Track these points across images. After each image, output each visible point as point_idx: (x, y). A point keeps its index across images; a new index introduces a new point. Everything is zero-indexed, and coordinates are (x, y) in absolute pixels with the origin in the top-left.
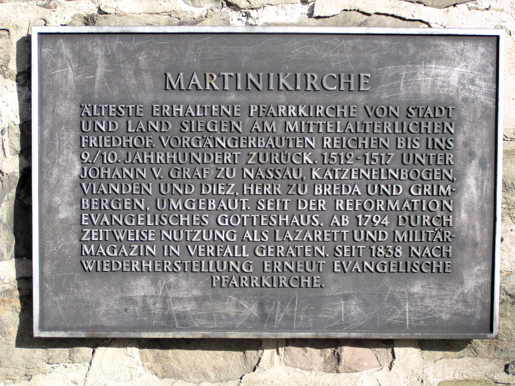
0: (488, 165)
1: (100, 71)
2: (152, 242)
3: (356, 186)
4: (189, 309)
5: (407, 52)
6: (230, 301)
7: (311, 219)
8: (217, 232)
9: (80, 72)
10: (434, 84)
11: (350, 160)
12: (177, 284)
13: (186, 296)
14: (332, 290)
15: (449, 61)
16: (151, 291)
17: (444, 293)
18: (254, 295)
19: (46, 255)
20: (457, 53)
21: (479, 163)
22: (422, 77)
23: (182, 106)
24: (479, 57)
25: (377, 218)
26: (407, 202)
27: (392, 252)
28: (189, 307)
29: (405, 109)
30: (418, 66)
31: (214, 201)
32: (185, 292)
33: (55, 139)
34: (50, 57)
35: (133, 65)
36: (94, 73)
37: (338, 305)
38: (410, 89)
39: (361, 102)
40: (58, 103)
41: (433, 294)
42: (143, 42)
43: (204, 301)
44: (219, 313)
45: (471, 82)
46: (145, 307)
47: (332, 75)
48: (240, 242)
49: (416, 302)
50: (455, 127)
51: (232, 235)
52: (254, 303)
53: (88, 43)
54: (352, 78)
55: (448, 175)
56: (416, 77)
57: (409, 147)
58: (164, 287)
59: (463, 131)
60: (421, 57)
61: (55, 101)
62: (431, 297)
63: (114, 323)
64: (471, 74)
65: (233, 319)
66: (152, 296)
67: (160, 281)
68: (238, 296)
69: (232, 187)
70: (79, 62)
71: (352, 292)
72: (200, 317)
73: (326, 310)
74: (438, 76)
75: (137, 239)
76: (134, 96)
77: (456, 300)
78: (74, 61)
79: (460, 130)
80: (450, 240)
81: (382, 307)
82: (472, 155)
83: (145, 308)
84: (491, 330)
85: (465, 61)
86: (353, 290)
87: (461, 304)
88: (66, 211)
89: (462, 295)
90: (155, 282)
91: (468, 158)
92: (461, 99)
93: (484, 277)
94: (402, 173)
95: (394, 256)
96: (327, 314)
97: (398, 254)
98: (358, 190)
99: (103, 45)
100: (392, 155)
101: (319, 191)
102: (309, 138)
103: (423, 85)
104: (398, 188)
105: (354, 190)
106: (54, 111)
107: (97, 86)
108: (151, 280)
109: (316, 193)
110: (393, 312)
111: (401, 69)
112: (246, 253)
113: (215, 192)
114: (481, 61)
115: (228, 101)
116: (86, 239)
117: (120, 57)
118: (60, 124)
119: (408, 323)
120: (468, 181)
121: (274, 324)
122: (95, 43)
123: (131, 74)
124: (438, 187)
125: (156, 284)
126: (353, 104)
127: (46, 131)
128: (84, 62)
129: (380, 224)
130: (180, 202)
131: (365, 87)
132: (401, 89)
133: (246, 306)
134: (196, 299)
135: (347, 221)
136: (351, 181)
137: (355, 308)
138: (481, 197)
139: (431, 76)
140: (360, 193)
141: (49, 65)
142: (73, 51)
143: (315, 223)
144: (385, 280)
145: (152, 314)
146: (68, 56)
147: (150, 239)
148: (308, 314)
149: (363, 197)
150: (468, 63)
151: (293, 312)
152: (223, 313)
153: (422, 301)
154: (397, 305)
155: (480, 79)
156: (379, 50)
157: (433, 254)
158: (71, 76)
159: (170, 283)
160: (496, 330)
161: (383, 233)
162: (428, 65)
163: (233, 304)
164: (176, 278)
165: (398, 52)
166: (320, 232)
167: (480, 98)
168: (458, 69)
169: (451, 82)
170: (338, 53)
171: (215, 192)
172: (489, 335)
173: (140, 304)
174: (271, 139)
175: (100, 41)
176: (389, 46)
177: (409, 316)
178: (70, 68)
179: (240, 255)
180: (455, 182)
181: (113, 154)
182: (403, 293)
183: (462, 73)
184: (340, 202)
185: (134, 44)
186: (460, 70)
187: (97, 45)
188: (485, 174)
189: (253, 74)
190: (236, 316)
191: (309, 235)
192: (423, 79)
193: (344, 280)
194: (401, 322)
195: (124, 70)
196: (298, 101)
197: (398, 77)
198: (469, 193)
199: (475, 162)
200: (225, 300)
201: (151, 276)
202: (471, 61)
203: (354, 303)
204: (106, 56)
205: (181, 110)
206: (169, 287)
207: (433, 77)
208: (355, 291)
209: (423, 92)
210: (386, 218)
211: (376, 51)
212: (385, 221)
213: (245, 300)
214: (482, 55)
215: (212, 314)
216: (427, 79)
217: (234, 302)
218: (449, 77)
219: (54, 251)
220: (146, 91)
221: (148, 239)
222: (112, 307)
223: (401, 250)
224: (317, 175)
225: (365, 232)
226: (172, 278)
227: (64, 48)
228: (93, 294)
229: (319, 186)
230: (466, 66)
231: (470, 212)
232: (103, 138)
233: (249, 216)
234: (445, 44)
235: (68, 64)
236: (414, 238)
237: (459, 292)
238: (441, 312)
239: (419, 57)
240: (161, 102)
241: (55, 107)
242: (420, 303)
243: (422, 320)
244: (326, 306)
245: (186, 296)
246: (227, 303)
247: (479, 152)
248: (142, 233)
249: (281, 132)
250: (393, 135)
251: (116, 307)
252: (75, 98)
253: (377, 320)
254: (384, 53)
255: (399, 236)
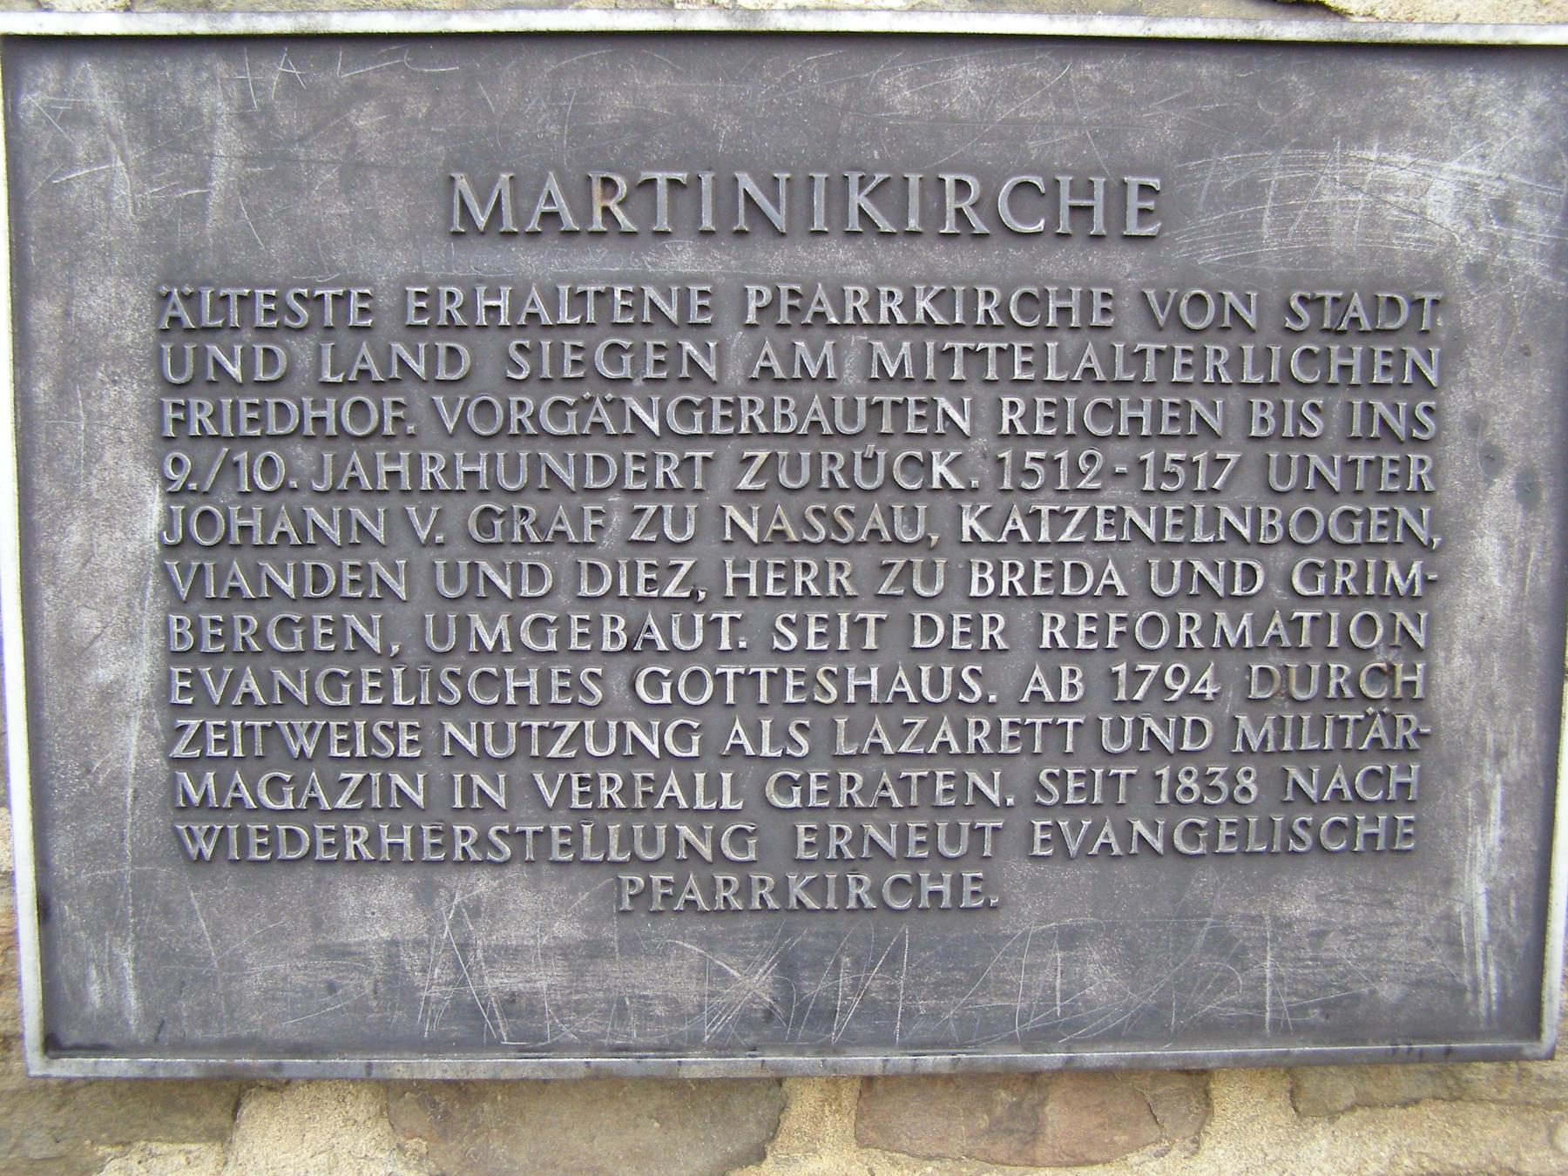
0: (1545, 495)
1: (223, 171)
2: (413, 764)
3: (1110, 566)
4: (542, 985)
5: (1286, 105)
6: (681, 957)
7: (957, 676)
8: (632, 727)
9: (154, 177)
10: (1373, 219)
11: (1090, 475)
12: (501, 903)
13: (532, 942)
14: (1027, 913)
15: (1429, 140)
16: (412, 924)
17: (1384, 915)
18: (760, 939)
19: (59, 807)
20: (1453, 109)
21: (1517, 486)
22: (1334, 191)
23: (506, 290)
24: (1525, 122)
25: (1178, 674)
26: (1277, 619)
27: (1223, 785)
28: (544, 980)
29: (1274, 299)
30: (1322, 155)
31: (622, 622)
32: (528, 928)
33: (73, 411)
34: (49, 123)
35: (335, 151)
36: (204, 180)
37: (1044, 966)
38: (1295, 235)
39: (1129, 276)
40: (80, 286)
41: (1352, 921)
42: (371, 69)
43: (592, 957)
44: (646, 997)
45: (1496, 213)
46: (396, 977)
47: (1032, 179)
48: (712, 761)
49: (1299, 948)
50: (1440, 364)
51: (683, 733)
52: (762, 964)
53: (182, 72)
54: (1099, 192)
55: (1415, 527)
56: (1313, 192)
57: (1288, 431)
58: (458, 914)
59: (1467, 379)
60: (1332, 122)
61: (70, 279)
62: (1345, 931)
63: (289, 1029)
64: (1497, 184)
65: (691, 1016)
66: (419, 943)
67: (443, 892)
68: (708, 942)
69: (683, 571)
70: (151, 141)
71: (1090, 919)
72: (579, 1008)
73: (1005, 982)
74: (1387, 190)
75: (361, 751)
76: (341, 258)
77: (1425, 939)
78: (133, 138)
79: (1455, 374)
80: (1413, 744)
81: (1187, 965)
82: (1492, 460)
83: (396, 985)
84: (1535, 1031)
85: (1480, 137)
86: (1093, 915)
87: (1440, 949)
88: (117, 658)
89: (1444, 923)
90: (425, 896)
91: (1482, 472)
92: (1461, 270)
93: (1518, 863)
94: (1265, 521)
95: (1231, 797)
96: (1004, 994)
97: (1245, 791)
98: (1117, 581)
99: (231, 80)
100: (1233, 457)
101: (983, 582)
102: (949, 399)
103: (1337, 219)
104: (1249, 571)
105: (1104, 582)
106: (67, 314)
107: (214, 219)
108: (413, 888)
109: (975, 591)
110: (1224, 981)
111: (1265, 165)
112: (734, 797)
113: (624, 591)
114: (1533, 140)
115: (669, 273)
116: (189, 754)
117: (288, 118)
118: (88, 360)
119: (1268, 1015)
120: (1478, 548)
121: (830, 1030)
122: (205, 75)
123: (331, 182)
124: (1382, 567)
125: (430, 902)
126: (1101, 283)
127: (41, 384)
128: (167, 137)
129: (1187, 694)
130: (502, 625)
131: (1141, 225)
132: (1266, 231)
133: (736, 974)
134: (565, 951)
135: (1079, 685)
136: (1090, 551)
137: (1099, 979)
138: (1518, 600)
139: (1365, 188)
140: (1121, 591)
141: (45, 151)
142: (128, 104)
143: (970, 691)
144: (1198, 881)
145: (419, 999)
146: (113, 119)
147: (403, 752)
148: (945, 994)
149: (1133, 602)
150: (1490, 145)
151: (893, 989)
152: (657, 997)
153: (1315, 947)
154: (1236, 959)
155: (1529, 200)
156: (1187, 99)
157: (1359, 790)
158: (123, 188)
159: (479, 898)
160: (1549, 1034)
161: (534, 568)
162: (1354, 153)
163: (692, 968)
164: (495, 884)
165: (1253, 104)
166: (987, 725)
167: (1526, 267)
168: (1454, 165)
169: (1429, 211)
170: (1051, 106)
171: (624, 591)
172: (1527, 1047)
173: (378, 969)
174: (816, 404)
175: (221, 67)
176: (1224, 83)
177: (1274, 993)
178: (120, 163)
179: (714, 805)
180: (1436, 551)
181: (269, 459)
182: (1257, 920)
183: (1466, 178)
184: (1054, 621)
185: (342, 72)
186: (1459, 168)
187: (213, 80)
188: (1534, 523)
189: (753, 175)
190: (701, 1007)
191: (946, 733)
192: (1337, 198)
193: (1063, 884)
194: (1246, 1012)
195: (308, 168)
196: (913, 270)
197: (1252, 191)
198: (1480, 587)
199: (1504, 484)
200: (664, 955)
201: (414, 877)
202: (1498, 139)
203: (1096, 957)
204: (243, 117)
205: (503, 303)
206: (475, 913)
207: (1370, 193)
208: (1099, 917)
209: (1336, 244)
210: (1208, 675)
211: (1178, 100)
212: (1204, 685)
213: (731, 953)
214: (1538, 116)
215: (621, 1002)
216: (1352, 198)
217: (695, 961)
218: (1425, 192)
219: (83, 793)
220: (388, 253)
221: (397, 749)
222: (285, 979)
223: (1255, 782)
224: (977, 527)
225: (1138, 723)
226: (483, 884)
227: (96, 90)
228: (218, 936)
229: (983, 567)
230: (1483, 157)
231: (1478, 653)
232: (235, 405)
233: (742, 671)
234: (1414, 78)
235: (113, 147)
236: (1297, 739)
237: (1437, 911)
238: (1377, 977)
239: (1324, 125)
240: (435, 275)
241: (71, 296)
242: (1310, 953)
243: (1314, 1006)
244: (1003, 970)
245: (532, 942)
246: (671, 964)
247: (1515, 452)
248: (377, 731)
249: (851, 378)
250: (1236, 390)
251: (300, 979)
252: (139, 268)
253: (1169, 1007)
254: (1206, 108)
255: (1250, 734)
